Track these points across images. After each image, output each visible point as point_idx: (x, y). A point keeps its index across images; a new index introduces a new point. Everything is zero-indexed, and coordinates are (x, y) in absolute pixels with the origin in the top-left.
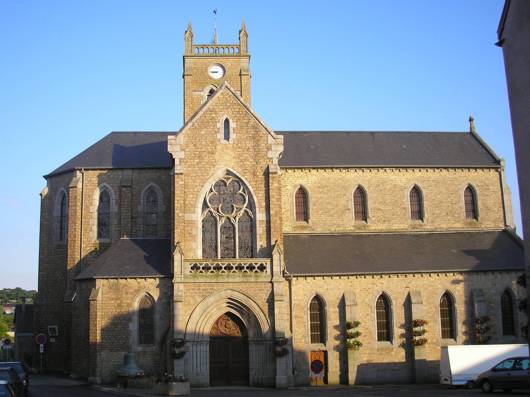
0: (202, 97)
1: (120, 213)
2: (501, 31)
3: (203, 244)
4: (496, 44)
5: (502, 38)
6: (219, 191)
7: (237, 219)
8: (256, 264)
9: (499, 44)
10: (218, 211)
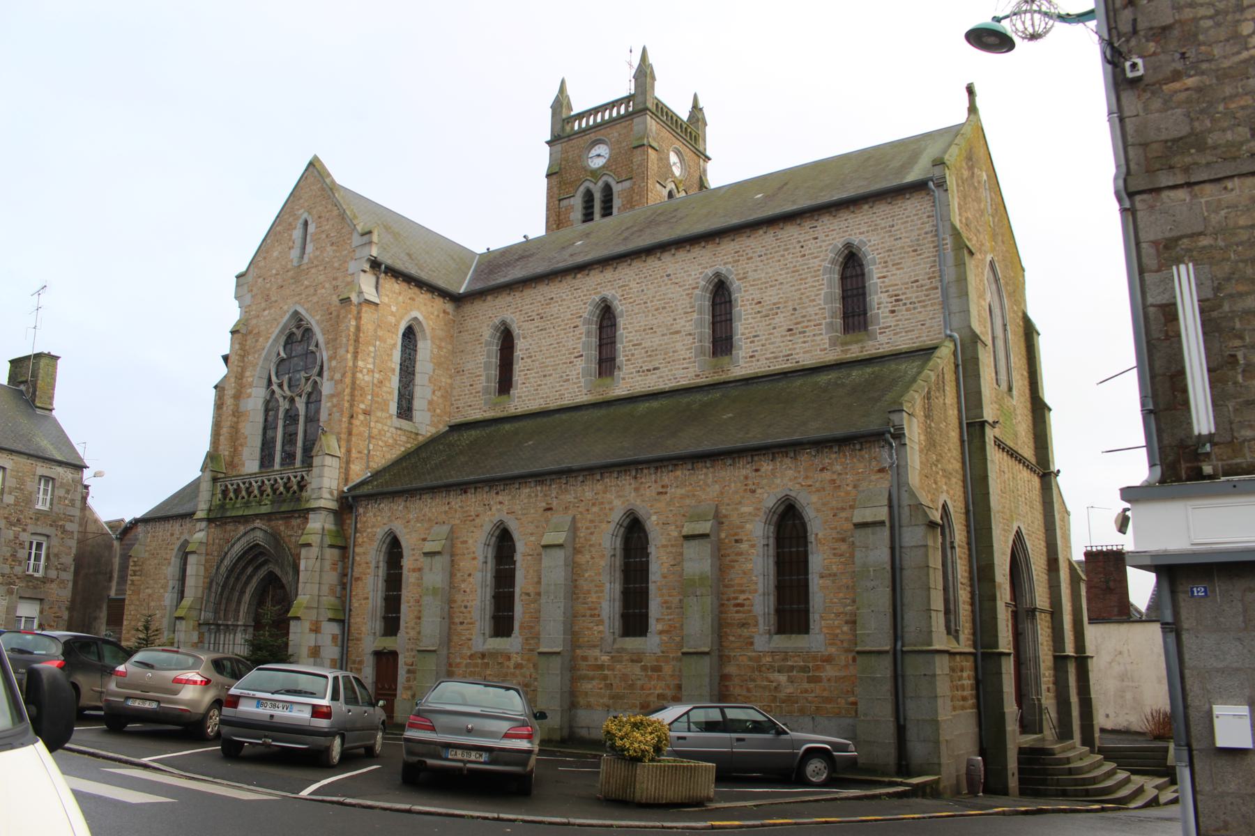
0: (572, 207)
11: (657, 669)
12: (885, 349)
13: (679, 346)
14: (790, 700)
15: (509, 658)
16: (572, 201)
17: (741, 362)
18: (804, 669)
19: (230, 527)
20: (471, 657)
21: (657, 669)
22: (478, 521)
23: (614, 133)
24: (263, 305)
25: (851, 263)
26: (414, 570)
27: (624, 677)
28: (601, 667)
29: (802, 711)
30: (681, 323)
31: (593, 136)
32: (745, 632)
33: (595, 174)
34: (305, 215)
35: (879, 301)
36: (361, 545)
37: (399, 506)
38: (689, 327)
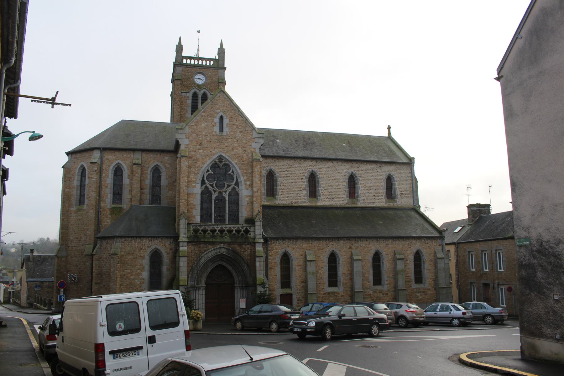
0: (188, 97)
1: (131, 185)
2: (500, 69)
3: (201, 212)
4: (495, 79)
5: (500, 75)
6: (214, 171)
7: (227, 193)
8: (242, 228)
9: (498, 79)
10: (213, 187)
11: (387, 294)
12: (399, 206)
13: (340, 193)
14: (421, 300)
15: (339, 294)
16: (188, 95)
17: (360, 202)
18: (424, 292)
19: (202, 246)
20: (324, 294)
21: (387, 294)
22: (324, 250)
23: (209, 73)
24: (198, 147)
25: (389, 180)
26: (298, 266)
27: (377, 297)
28: (370, 295)
29: (424, 302)
30: (341, 186)
31: (198, 70)
32: (410, 283)
33: (199, 86)
34: (221, 114)
35: (398, 193)
36: (271, 256)
37: (290, 243)
38: (343, 188)
